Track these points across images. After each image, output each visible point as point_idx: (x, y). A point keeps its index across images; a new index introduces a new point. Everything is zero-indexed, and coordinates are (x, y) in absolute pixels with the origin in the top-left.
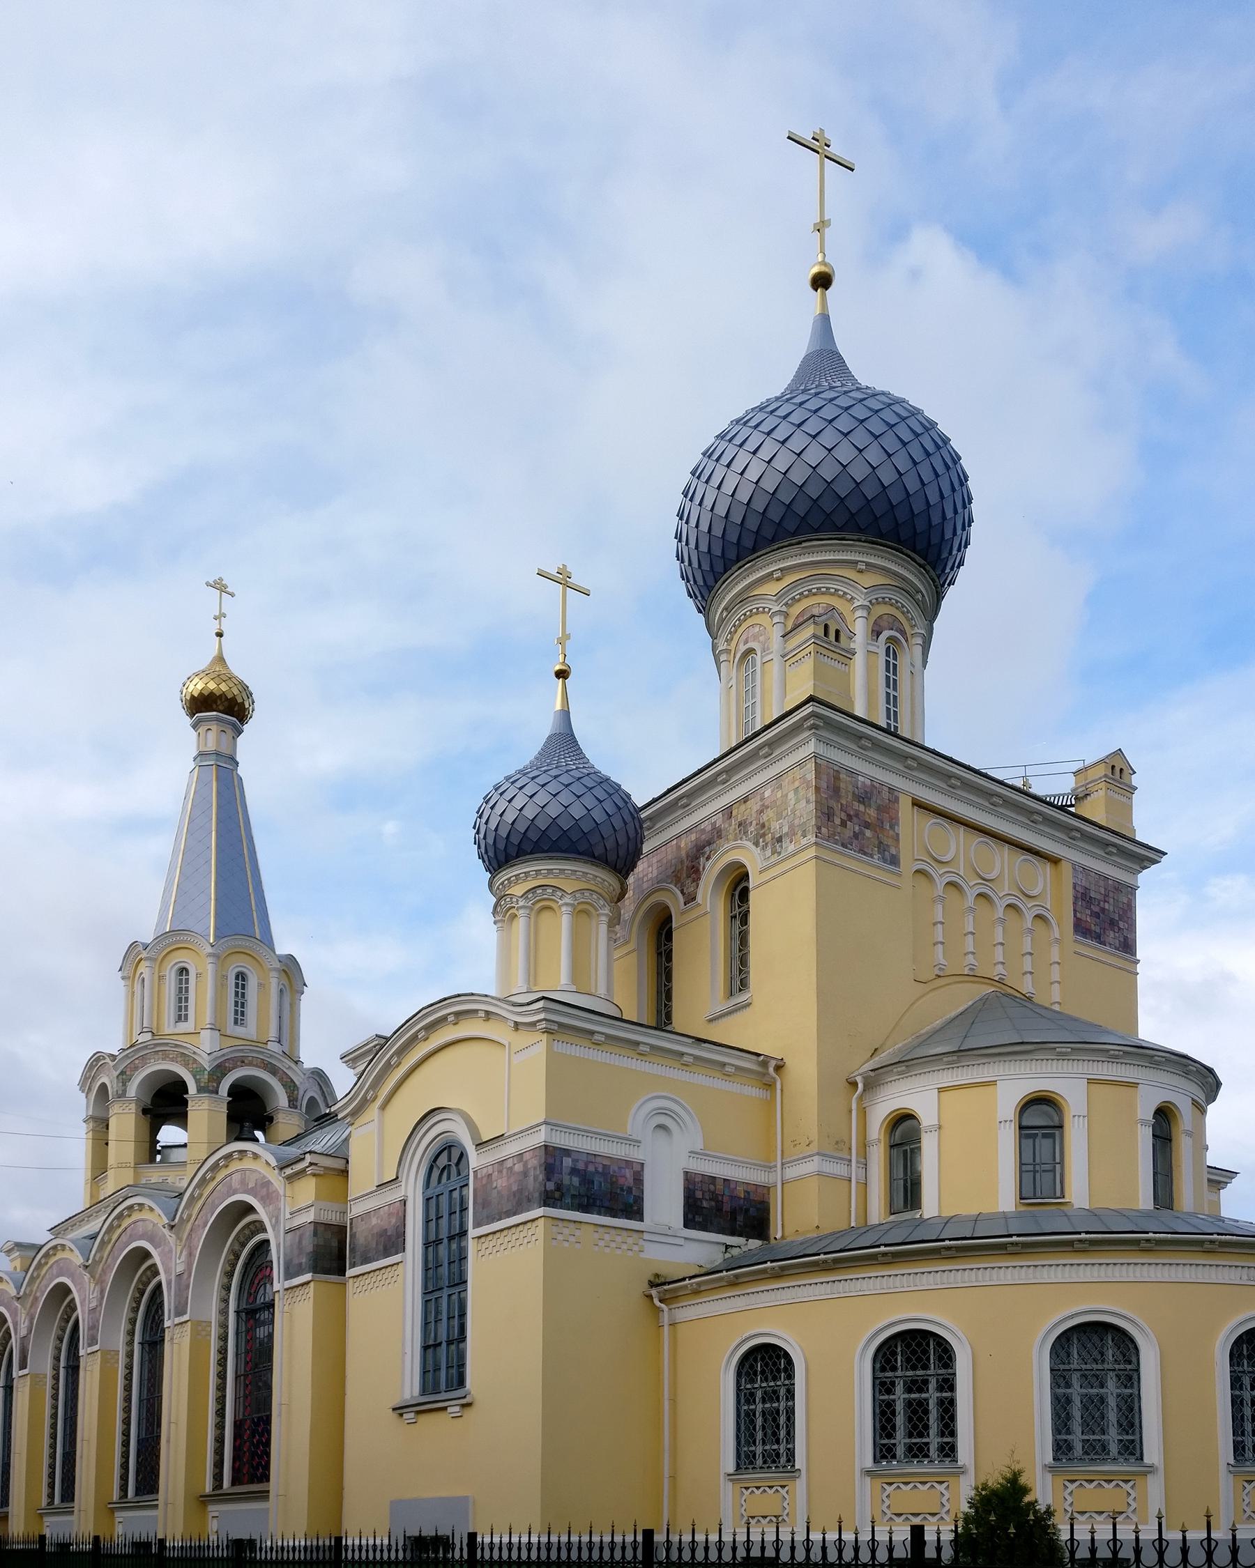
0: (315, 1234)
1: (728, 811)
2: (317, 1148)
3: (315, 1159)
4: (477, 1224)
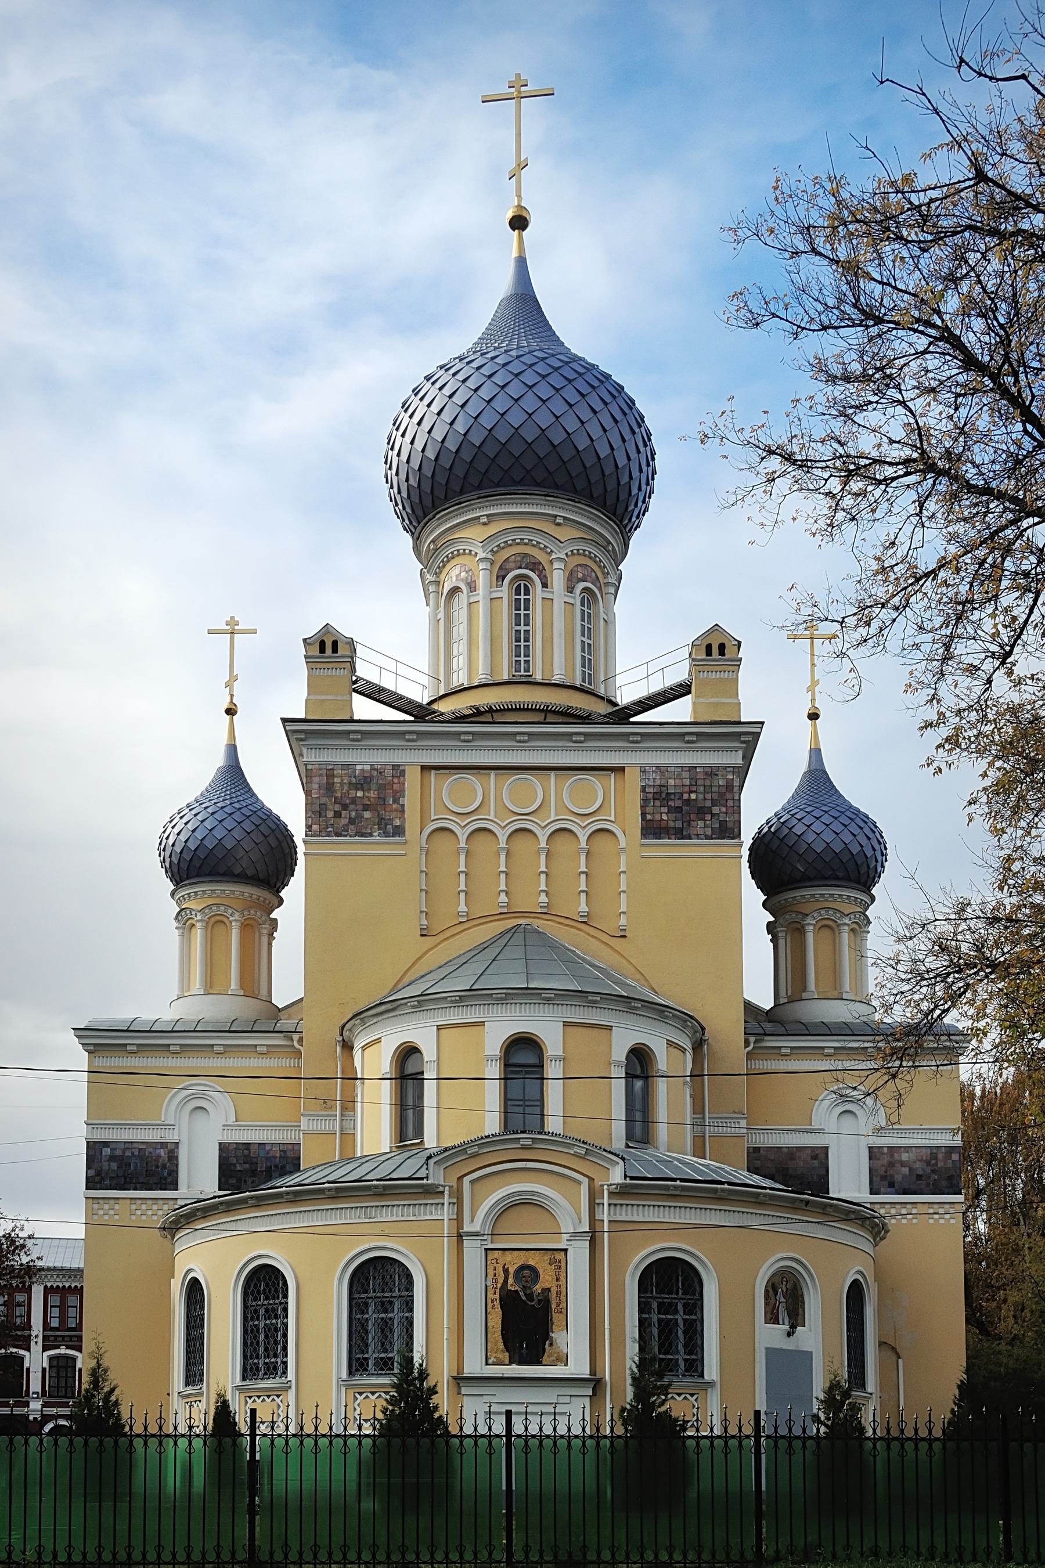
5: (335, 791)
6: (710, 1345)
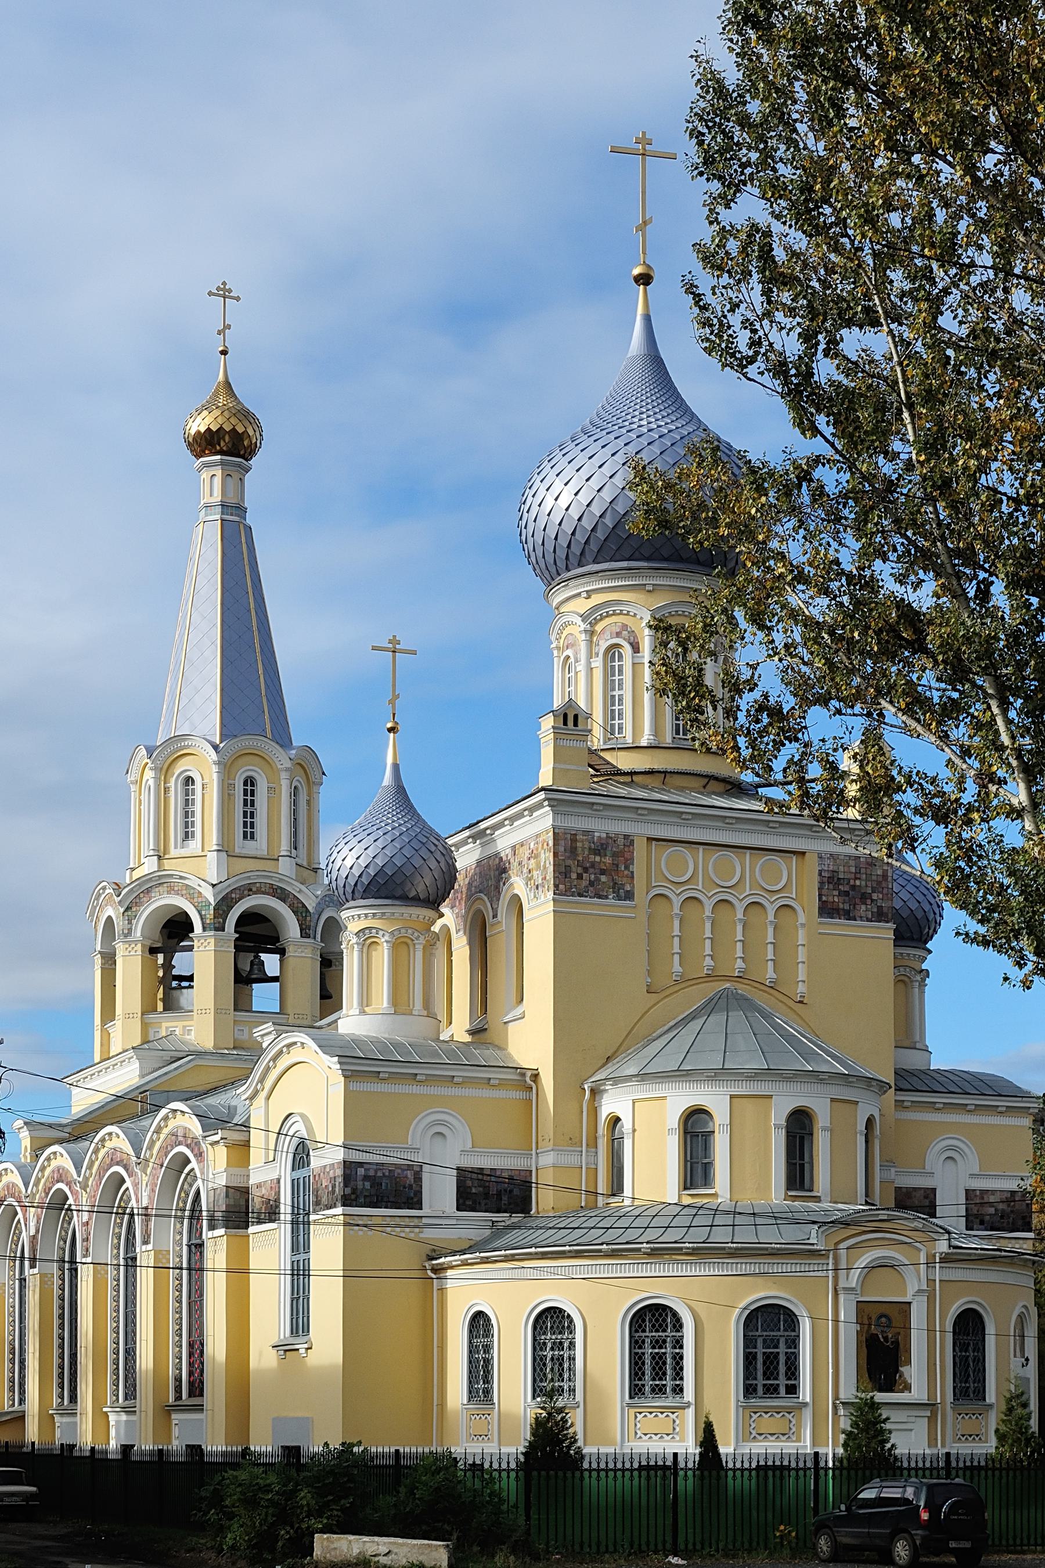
0: (227, 1196)
5: (577, 855)
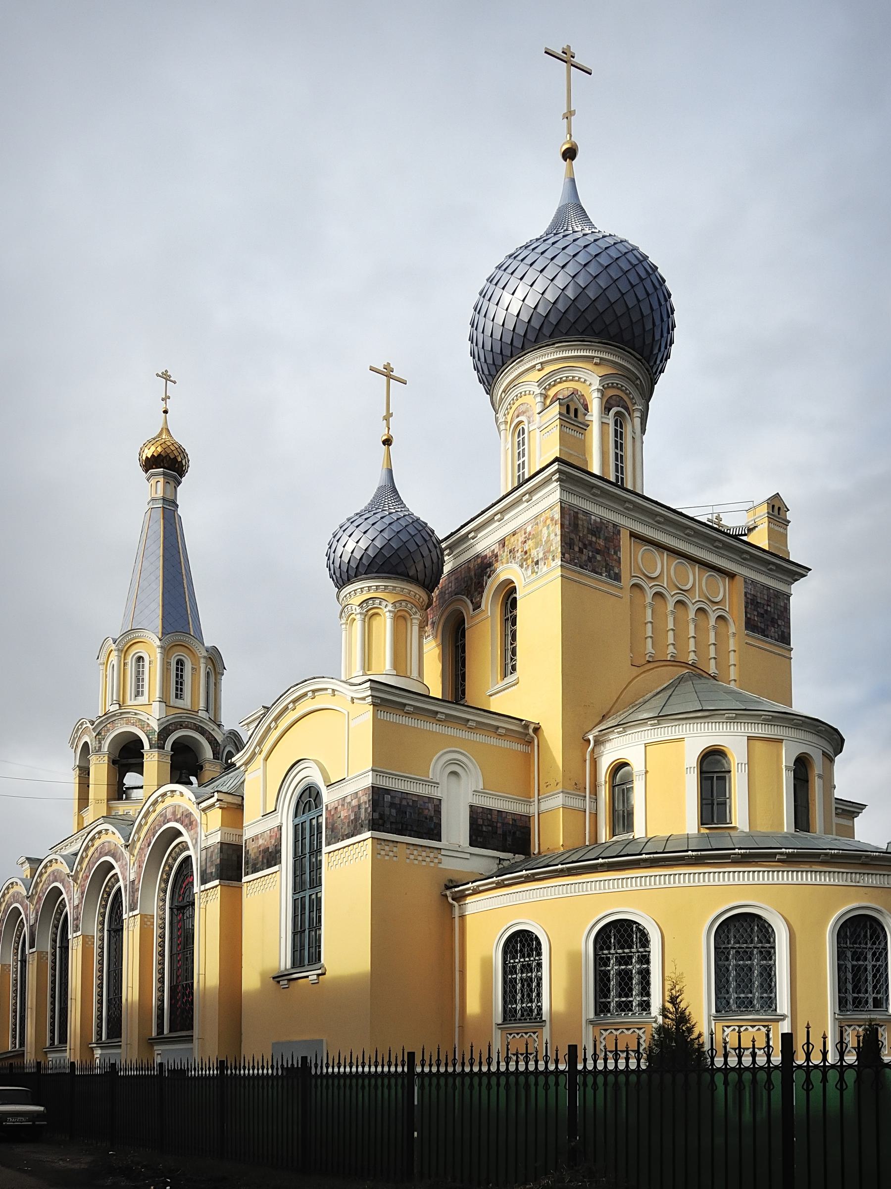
0: (221, 852)
1: (503, 543)
2: (224, 789)
3: (222, 796)
4: (328, 844)
6: (781, 1002)
